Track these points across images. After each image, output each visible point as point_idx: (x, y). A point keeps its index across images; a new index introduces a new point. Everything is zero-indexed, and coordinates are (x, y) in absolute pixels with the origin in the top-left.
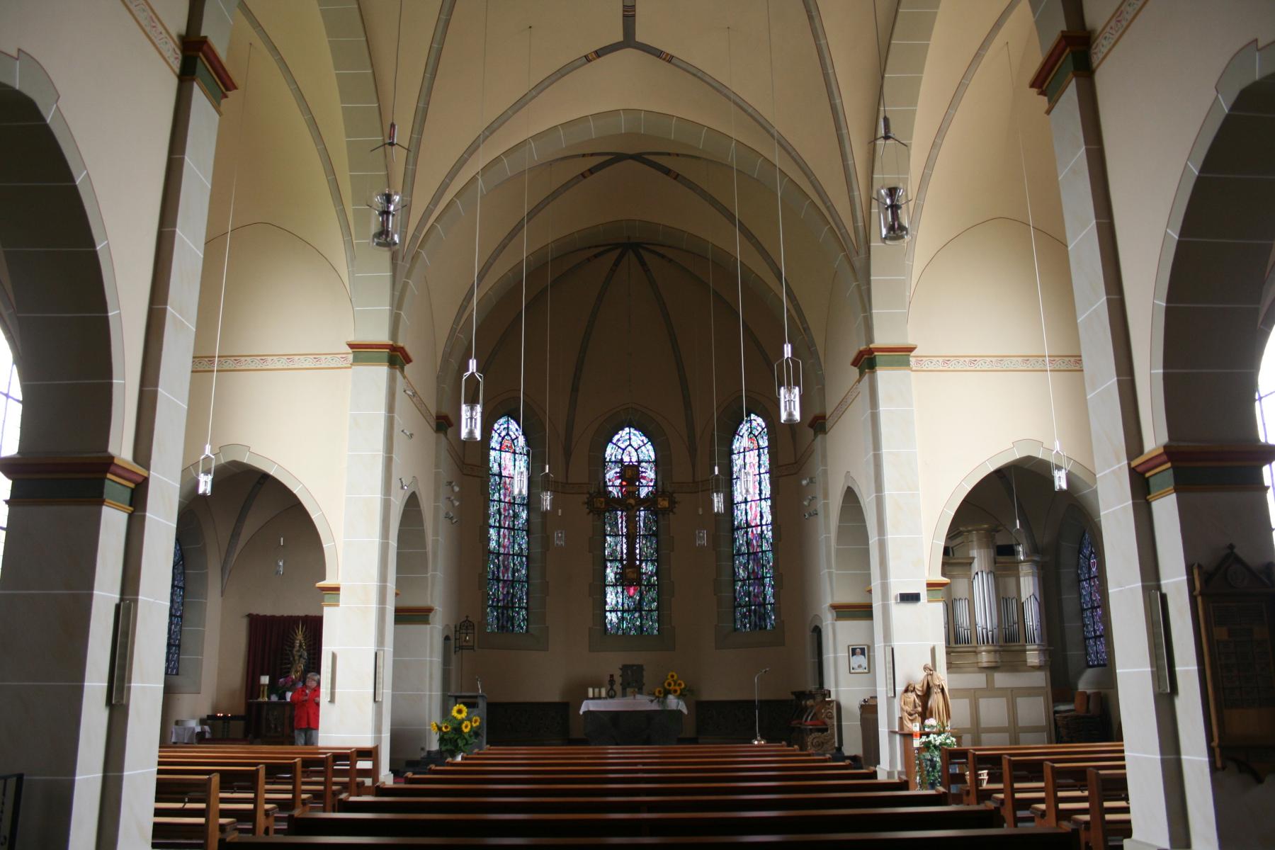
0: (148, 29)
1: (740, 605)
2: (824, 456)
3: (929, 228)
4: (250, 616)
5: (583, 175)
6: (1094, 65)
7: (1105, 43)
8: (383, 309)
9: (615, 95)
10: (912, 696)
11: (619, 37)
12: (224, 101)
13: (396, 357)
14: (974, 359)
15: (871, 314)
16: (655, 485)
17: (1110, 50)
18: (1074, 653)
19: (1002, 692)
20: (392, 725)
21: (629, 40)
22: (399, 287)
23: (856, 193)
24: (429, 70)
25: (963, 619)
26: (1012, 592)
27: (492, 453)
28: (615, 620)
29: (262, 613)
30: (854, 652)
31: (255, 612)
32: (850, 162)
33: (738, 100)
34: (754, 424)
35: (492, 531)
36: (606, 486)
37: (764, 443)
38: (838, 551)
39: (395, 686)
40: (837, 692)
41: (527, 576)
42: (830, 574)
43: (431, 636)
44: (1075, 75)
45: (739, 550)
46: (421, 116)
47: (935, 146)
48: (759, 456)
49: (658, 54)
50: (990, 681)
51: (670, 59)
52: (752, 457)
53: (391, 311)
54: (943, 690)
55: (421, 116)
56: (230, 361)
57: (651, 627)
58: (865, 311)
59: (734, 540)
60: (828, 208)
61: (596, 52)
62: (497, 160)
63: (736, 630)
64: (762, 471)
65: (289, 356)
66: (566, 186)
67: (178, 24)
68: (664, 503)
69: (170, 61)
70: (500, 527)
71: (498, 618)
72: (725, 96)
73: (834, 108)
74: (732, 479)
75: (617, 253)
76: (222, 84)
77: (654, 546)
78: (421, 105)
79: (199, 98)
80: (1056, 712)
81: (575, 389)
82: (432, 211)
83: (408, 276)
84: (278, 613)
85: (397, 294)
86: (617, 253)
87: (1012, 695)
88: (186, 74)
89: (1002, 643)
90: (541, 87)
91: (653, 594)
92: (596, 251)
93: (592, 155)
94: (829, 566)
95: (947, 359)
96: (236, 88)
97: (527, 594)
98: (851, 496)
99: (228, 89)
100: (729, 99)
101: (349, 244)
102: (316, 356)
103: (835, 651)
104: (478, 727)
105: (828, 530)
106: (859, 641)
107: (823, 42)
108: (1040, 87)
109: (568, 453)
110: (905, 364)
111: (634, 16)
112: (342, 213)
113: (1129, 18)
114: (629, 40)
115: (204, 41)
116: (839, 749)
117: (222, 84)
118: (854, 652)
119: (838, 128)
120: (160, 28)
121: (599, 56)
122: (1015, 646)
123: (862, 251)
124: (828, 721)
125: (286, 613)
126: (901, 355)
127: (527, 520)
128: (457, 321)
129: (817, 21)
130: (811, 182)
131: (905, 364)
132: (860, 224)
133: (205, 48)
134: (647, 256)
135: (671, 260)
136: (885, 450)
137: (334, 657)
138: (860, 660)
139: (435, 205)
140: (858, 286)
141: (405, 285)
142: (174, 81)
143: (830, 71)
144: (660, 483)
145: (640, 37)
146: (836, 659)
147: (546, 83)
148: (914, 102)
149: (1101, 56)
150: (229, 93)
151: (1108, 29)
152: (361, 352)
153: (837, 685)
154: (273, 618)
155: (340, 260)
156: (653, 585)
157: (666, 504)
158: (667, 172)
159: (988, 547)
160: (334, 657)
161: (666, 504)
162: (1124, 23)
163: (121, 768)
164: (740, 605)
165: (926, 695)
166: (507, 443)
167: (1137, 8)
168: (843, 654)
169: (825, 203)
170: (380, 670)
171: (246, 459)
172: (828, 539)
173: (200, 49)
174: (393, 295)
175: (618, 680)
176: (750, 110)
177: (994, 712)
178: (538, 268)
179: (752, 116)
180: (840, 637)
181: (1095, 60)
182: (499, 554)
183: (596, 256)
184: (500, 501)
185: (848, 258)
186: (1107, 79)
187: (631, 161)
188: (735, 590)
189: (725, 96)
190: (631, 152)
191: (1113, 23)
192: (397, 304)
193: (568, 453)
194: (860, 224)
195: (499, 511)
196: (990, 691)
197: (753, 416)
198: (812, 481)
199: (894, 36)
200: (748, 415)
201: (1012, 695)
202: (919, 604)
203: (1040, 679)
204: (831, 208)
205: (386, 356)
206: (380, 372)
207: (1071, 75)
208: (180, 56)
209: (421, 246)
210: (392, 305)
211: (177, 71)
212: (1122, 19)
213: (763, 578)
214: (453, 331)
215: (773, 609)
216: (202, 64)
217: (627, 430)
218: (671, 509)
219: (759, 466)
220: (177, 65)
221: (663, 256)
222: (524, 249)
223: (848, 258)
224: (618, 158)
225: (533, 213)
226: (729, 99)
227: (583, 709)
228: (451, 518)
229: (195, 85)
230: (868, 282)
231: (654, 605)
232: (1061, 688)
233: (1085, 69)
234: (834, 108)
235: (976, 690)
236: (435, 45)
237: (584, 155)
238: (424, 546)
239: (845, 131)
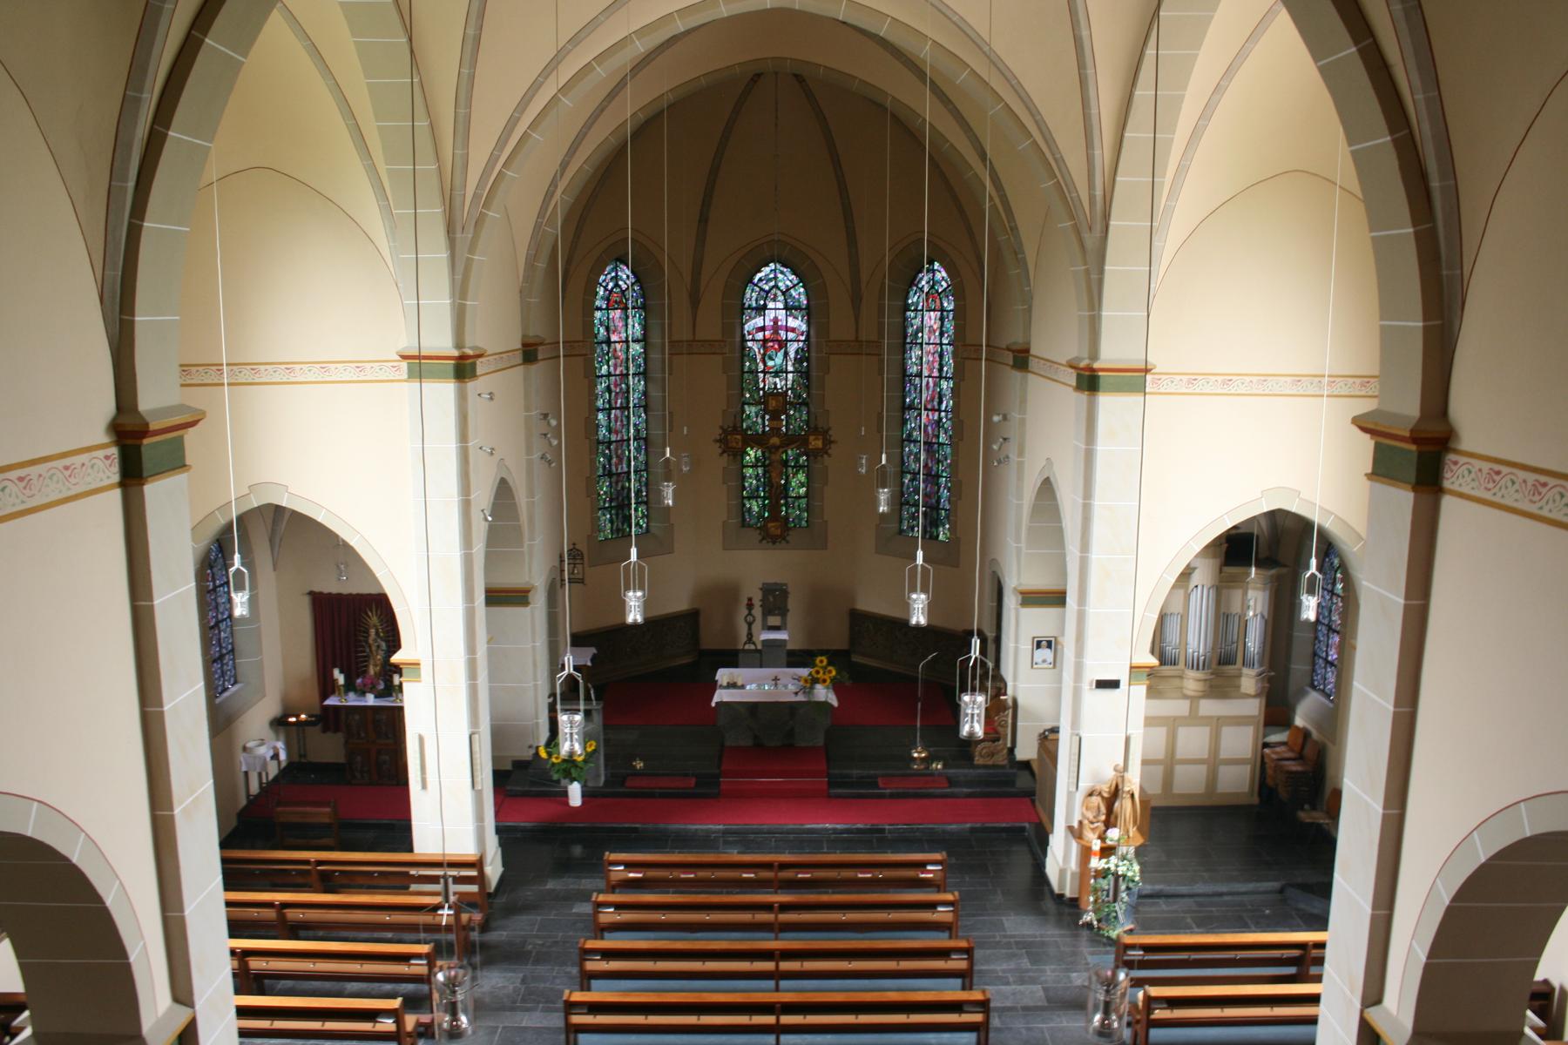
1: (908, 503)
2: (1024, 401)
3: (1186, 207)
4: (311, 593)
8: (439, 303)
10: (1096, 800)
13: (463, 369)
14: (1228, 379)
15: (1100, 316)
16: (807, 339)
18: (1299, 667)
19: (1206, 721)
20: (492, 719)
22: (460, 268)
23: (1097, 152)
25: (1173, 636)
26: (1236, 608)
27: (598, 314)
28: (756, 509)
29: (326, 591)
30: (1039, 645)
31: (317, 589)
32: (1094, 111)
34: (938, 276)
35: (600, 416)
36: (744, 340)
37: (949, 305)
38: (1029, 529)
39: (492, 677)
40: (1015, 687)
41: (646, 463)
42: (1019, 550)
43: (531, 621)
45: (910, 435)
46: (472, 45)
47: (1219, 90)
48: (942, 319)
50: (1194, 709)
52: (932, 319)
53: (453, 304)
54: (1132, 796)
55: (472, 45)
56: (246, 371)
57: (799, 518)
58: (1092, 308)
59: (904, 422)
62: (588, 68)
63: (901, 532)
64: (945, 341)
65: (323, 364)
68: (816, 443)
70: (611, 408)
71: (611, 521)
73: (1078, 41)
74: (905, 343)
77: (805, 417)
78: (471, 32)
80: (1265, 745)
81: (704, 220)
83: (472, 250)
84: (345, 590)
85: (459, 277)
87: (1217, 724)
89: (1214, 666)
91: (801, 477)
94: (1018, 540)
95: (1193, 378)
97: (647, 485)
98: (1047, 488)
101: (386, 210)
102: (359, 364)
103: (1017, 641)
104: (594, 751)
105: (1020, 497)
106: (1045, 632)
109: (695, 299)
110: (1141, 388)
112: (372, 169)
116: (1011, 750)
118: (1039, 645)
119: (1081, 65)
122: (1229, 669)
123: (1098, 227)
124: (1000, 729)
125: (354, 591)
126: (1135, 379)
127: (645, 393)
128: (541, 215)
131: (1141, 388)
132: (1099, 193)
136: (1098, 503)
137: (421, 739)
138: (1045, 654)
139: (502, 150)
141: (469, 262)
144: (813, 340)
146: (1016, 649)
152: (419, 365)
153: (1015, 678)
154: (339, 595)
156: (802, 467)
157: (819, 444)
159: (1214, 557)
160: (421, 739)
161: (819, 444)
163: (180, 907)
164: (908, 503)
165: (1116, 793)
166: (615, 297)
168: (1026, 646)
170: (477, 756)
171: (284, 502)
172: (1020, 507)
174: (453, 281)
175: (757, 603)
176: (955, 19)
177: (1193, 742)
180: (1022, 626)
182: (610, 443)
184: (609, 375)
188: (902, 484)
192: (461, 291)
193: (695, 299)
194: (1099, 193)
195: (608, 389)
196: (1193, 719)
197: (936, 265)
198: (1005, 418)
200: (931, 262)
201: (1217, 724)
202: (1117, 691)
203: (1253, 707)
204: (1060, 161)
205: (451, 370)
206: (443, 392)
210: (453, 295)
213: (938, 476)
214: (537, 226)
215: (947, 517)
217: (772, 266)
218: (824, 451)
219: (942, 334)
223: (1077, 230)
227: (716, 699)
228: (550, 462)
230: (1101, 271)
231: (803, 491)
232: (1277, 712)
234: (1078, 41)
235: (1175, 719)
238: (517, 518)
239: (1090, 71)
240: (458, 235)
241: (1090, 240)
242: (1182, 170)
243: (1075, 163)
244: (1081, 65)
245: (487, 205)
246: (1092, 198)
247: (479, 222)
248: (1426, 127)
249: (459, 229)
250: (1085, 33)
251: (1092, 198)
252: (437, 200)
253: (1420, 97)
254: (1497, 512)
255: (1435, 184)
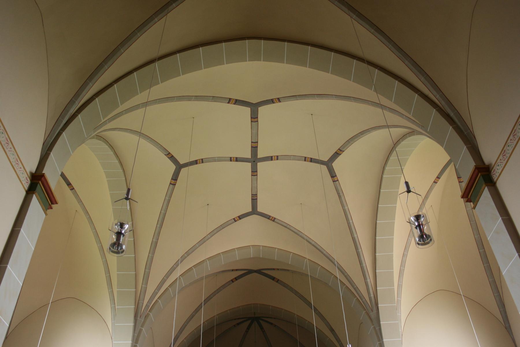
0: (14, 164)
5: (232, 281)
6: (495, 180)
7: (498, 167)
9: (249, 238)
11: (250, 209)
12: (49, 211)
15: (383, 342)
17: (500, 175)
21: (254, 211)
23: (368, 280)
24: (160, 222)
32: (364, 265)
33: (308, 239)
44: (487, 185)
47: (404, 255)
49: (268, 217)
51: (274, 220)
53: (132, 344)
58: (379, 340)
60: (355, 289)
61: (239, 217)
62: (191, 269)
66: (224, 286)
67: (32, 167)
69: (23, 183)
72: (301, 236)
75: (249, 322)
76: (50, 201)
78: (154, 240)
79: (35, 202)
82: (157, 293)
83: (142, 326)
85: (136, 335)
86: (249, 322)
88: (30, 191)
90: (212, 233)
92: (239, 321)
93: (237, 270)
96: (57, 203)
99: (52, 203)
100: (304, 238)
101: (114, 309)
107: (346, 208)
108: (467, 197)
111: (257, 199)
113: (500, 171)
114: (254, 211)
115: (43, 175)
117: (50, 201)
119: (356, 248)
120: (21, 165)
121: (240, 219)
123: (375, 309)
129: (343, 198)
130: (345, 276)
132: (372, 296)
133: (43, 179)
134: (265, 325)
135: (275, 326)
140: (375, 328)
141: (141, 330)
142: (24, 193)
143: (351, 221)
145: (260, 209)
147: (215, 232)
148: (392, 234)
149: (498, 174)
150: (53, 206)
151: (499, 161)
155: (108, 316)
158: (273, 278)
162: (508, 155)
167: (514, 146)
169: (353, 287)
173: (40, 180)
174: (134, 336)
176: (313, 243)
178: (209, 329)
179: (313, 245)
181: (495, 178)
183: (238, 324)
185: (368, 314)
186: (502, 185)
187: (255, 273)
189: (301, 236)
190: (255, 269)
191: (501, 157)
194: (372, 296)
199: (380, 203)
204: (356, 289)
207: (484, 185)
208: (29, 182)
209: (150, 311)
210: (133, 341)
211: (27, 189)
212: (505, 154)
216: (40, 187)
220: (27, 186)
221: (272, 324)
222: (202, 319)
223: (368, 314)
224: (250, 272)
225: (207, 300)
226: (304, 238)
229: (34, 195)
230: (380, 325)
233: (491, 183)
234: (349, 224)
236: (163, 212)
237: (233, 270)
239: (360, 250)
240: (138, 318)
241: (373, 315)
242: (400, 286)
243: (362, 288)
244: (356, 248)
245: (150, 311)
246: (370, 298)
247: (147, 317)
248: (443, 103)
249: (139, 316)
250: (355, 236)
251: (370, 298)
252: (133, 302)
253: (438, 96)
254: (514, 153)
255: (452, 115)
